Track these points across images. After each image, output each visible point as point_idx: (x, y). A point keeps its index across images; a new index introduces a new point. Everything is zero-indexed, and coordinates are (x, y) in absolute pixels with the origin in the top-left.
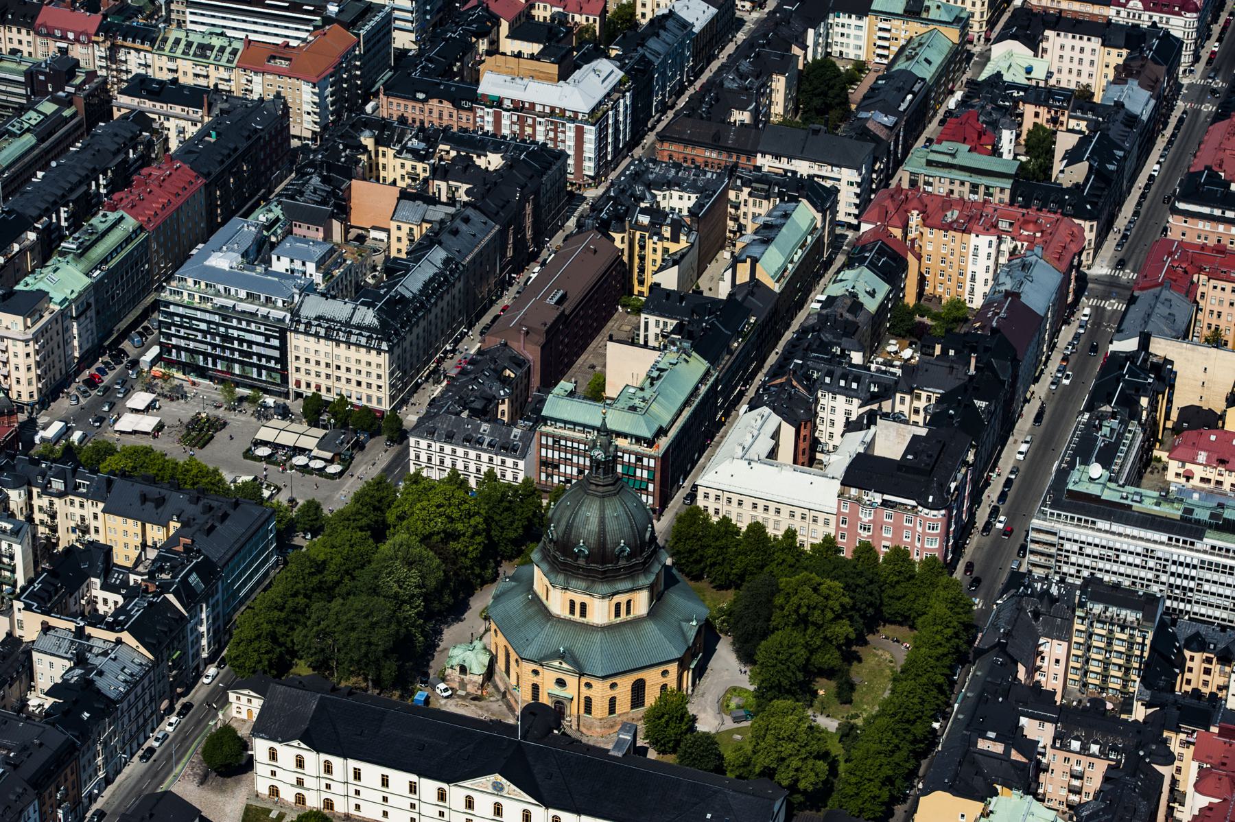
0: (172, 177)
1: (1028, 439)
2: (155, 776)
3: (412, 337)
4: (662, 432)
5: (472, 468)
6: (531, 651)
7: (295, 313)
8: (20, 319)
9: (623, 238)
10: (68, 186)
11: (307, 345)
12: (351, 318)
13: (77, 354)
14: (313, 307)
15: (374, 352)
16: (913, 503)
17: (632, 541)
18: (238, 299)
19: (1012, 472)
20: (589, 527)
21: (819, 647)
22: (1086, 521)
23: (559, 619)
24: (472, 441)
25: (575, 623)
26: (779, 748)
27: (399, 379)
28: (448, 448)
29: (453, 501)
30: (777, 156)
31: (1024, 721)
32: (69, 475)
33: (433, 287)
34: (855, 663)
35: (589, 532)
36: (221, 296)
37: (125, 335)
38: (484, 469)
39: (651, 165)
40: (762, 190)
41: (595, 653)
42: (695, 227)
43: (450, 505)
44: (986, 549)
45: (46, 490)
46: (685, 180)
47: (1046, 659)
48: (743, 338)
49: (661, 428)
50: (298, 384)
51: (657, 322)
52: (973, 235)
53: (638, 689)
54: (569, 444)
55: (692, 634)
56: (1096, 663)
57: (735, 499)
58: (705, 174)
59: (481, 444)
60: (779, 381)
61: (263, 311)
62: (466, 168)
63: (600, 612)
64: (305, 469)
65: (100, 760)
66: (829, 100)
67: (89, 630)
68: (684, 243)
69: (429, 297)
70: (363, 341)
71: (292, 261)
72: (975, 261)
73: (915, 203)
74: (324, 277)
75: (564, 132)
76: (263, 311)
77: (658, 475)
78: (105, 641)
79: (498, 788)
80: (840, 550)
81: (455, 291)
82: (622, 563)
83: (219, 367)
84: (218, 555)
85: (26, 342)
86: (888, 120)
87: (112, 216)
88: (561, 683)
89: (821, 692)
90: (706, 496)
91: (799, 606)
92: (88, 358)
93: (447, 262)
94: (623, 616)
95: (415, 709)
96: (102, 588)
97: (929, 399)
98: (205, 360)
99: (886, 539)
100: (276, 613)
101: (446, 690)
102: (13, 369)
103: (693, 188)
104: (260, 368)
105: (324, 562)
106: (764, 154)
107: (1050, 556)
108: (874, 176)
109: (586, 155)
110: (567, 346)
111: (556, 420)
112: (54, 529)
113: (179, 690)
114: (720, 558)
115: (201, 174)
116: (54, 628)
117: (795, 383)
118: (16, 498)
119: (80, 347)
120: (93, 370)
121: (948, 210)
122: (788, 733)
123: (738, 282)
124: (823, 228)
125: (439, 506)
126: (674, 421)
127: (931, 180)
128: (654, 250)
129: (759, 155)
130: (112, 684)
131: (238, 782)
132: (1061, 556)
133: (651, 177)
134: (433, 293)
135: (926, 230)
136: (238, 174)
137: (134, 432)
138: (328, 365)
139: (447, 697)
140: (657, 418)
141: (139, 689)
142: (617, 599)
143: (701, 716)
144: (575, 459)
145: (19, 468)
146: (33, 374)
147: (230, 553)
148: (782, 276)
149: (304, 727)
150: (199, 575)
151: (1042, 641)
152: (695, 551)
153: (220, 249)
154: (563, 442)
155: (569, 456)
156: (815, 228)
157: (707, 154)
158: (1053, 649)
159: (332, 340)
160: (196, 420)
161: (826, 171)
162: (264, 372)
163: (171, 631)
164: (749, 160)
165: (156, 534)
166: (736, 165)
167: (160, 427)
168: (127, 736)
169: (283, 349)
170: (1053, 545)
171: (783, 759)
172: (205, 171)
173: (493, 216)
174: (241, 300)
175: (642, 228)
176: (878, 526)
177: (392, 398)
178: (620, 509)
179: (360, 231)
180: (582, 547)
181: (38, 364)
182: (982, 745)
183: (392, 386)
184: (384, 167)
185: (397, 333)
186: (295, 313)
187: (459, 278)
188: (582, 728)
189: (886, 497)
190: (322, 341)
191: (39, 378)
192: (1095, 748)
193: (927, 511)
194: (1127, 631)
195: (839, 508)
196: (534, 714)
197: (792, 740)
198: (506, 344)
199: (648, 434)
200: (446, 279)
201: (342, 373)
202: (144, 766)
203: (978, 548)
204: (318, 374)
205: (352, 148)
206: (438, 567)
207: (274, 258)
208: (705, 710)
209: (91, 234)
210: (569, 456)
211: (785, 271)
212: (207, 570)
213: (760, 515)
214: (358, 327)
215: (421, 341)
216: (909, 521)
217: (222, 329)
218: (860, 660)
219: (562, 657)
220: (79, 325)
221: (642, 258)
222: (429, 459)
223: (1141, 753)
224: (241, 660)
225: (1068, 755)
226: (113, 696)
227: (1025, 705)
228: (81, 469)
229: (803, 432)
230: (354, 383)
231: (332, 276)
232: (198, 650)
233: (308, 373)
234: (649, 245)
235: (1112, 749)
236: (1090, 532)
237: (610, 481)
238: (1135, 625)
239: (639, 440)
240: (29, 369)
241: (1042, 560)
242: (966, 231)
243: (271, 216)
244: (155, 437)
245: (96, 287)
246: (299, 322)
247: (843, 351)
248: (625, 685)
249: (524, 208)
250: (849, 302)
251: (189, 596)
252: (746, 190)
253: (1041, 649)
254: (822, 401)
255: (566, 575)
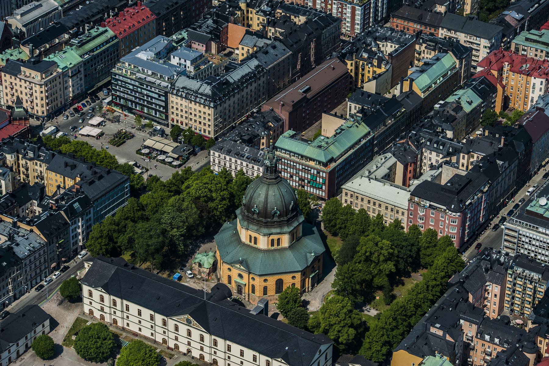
0: (139, 14)
1: (535, 185)
2: (40, 299)
3: (231, 102)
4: (332, 160)
5: (233, 167)
6: (228, 258)
7: (173, 84)
8: (39, 74)
9: (352, 64)
10: (91, 14)
11: (177, 101)
12: (199, 90)
13: (71, 95)
14: (182, 82)
15: (207, 107)
16: (445, 208)
17: (281, 208)
18: (147, 75)
19: (520, 201)
20: (260, 199)
21: (377, 274)
22: (534, 227)
23: (244, 244)
24: (239, 155)
25: (252, 247)
26: (330, 320)
27: (221, 123)
28: (228, 158)
29: (213, 182)
30: (449, 30)
31: (462, 321)
32: (36, 150)
33: (246, 79)
34: (400, 286)
35: (260, 202)
36: (140, 73)
37: (100, 89)
38: (239, 168)
39: (379, 28)
40: (433, 46)
41: (257, 262)
42: (390, 61)
43: (211, 184)
44: (491, 237)
45: (24, 157)
46: (394, 37)
47: (490, 294)
48: (395, 119)
49: (333, 158)
50: (173, 120)
51: (355, 107)
52: (533, 78)
53: (279, 283)
54: (286, 161)
55: (310, 260)
56: (517, 299)
57: (360, 197)
58: (405, 35)
59: (243, 157)
60: (402, 141)
61: (158, 82)
62: (285, 22)
63: (263, 243)
64: (163, 161)
65: (10, 287)
66: (497, 4)
67: (19, 224)
68: (383, 69)
69: (242, 83)
70: (202, 101)
71: (180, 59)
72: (533, 92)
73: (507, 58)
74: (195, 68)
75: (346, 9)
76: (158, 82)
77: (327, 182)
78: (26, 230)
79: (189, 322)
80: (403, 228)
81: (261, 82)
82: (276, 219)
83: (138, 109)
84: (93, 196)
85: (41, 85)
86: (518, 16)
87: (101, 29)
88: (240, 276)
89: (378, 298)
90: (346, 194)
91: (366, 252)
92: (78, 98)
93: (257, 67)
94: (276, 246)
95: (172, 283)
96: (38, 206)
97: (478, 157)
98: (132, 104)
99: (431, 225)
100: (114, 227)
101: (190, 274)
102: (34, 98)
103: (398, 42)
104: (156, 110)
105: (146, 205)
106: (443, 28)
107: (515, 243)
108: (502, 45)
109: (357, 22)
110: (308, 114)
111: (282, 149)
112: (28, 176)
113: (63, 259)
114: (343, 225)
115: (153, 13)
116: (4, 221)
117: (410, 143)
118: (10, 159)
119: (73, 92)
120: (80, 104)
121: (524, 64)
122: (335, 312)
123: (403, 91)
124: (461, 68)
125: (205, 184)
126: (341, 155)
127: (526, 48)
128: (369, 71)
129: (440, 29)
130: (22, 251)
131: (77, 306)
132: (519, 244)
133: (377, 34)
134: (246, 81)
135: (511, 73)
136: (177, 16)
137: (88, 136)
138: (186, 112)
139: (191, 278)
140: (332, 152)
141: (37, 255)
142: (272, 237)
143: (313, 302)
144: (289, 170)
145: (15, 144)
146: (44, 102)
147: (100, 195)
148: (428, 90)
149: (106, 281)
150: (79, 204)
151: (488, 284)
152: (332, 220)
153: (146, 50)
154: (283, 160)
155: (286, 168)
156: (455, 67)
157: (415, 26)
158: (494, 289)
159: (188, 99)
160: (119, 132)
161: (473, 39)
162: (158, 113)
163: (59, 229)
164: (435, 31)
165: (70, 183)
166: (421, 32)
167: (101, 135)
168: (29, 277)
169: (166, 102)
170: (515, 238)
171: (332, 325)
172: (157, 12)
173: (290, 47)
174: (149, 76)
175: (364, 59)
176: (426, 217)
177: (215, 132)
178: (277, 192)
179: (231, 50)
180: (255, 209)
181: (47, 97)
182: (433, 330)
183: (216, 126)
184: (251, 19)
185: (220, 99)
186: (173, 84)
187: (263, 76)
188: (251, 301)
189: (432, 203)
190: (184, 99)
191: (48, 104)
192: (497, 340)
193: (450, 213)
194: (533, 284)
195: (409, 207)
196: (218, 289)
197: (338, 316)
198: (272, 110)
199: (324, 160)
200: (255, 75)
201: (192, 117)
202: (37, 293)
203: (487, 237)
204: (204, 118)
205: (233, 7)
206: (195, 213)
207: (172, 57)
208: (315, 299)
209: (88, 37)
210: (286, 168)
211: (430, 87)
212: (85, 202)
213: (365, 206)
214: (201, 94)
215: (236, 106)
216: (442, 217)
217: (139, 89)
218: (403, 284)
219: (241, 263)
220: (73, 81)
221: (363, 75)
222: (219, 162)
223: (517, 345)
224: (92, 248)
225: (484, 342)
226: (21, 256)
227: (464, 313)
228: (43, 148)
229: (410, 168)
230: (198, 122)
231: (200, 69)
232: (76, 241)
233: (177, 115)
234: (367, 69)
235: (505, 342)
236: (534, 233)
237: (273, 177)
238: (537, 281)
239: (320, 163)
240: (42, 99)
241: (511, 245)
242: (529, 75)
243: (180, 37)
244: (97, 139)
245: (85, 63)
246: (174, 89)
247: (443, 130)
248: (272, 281)
249: (310, 45)
250: (454, 106)
251: (71, 212)
252: (424, 45)
253: (488, 288)
254: (425, 154)
255: (248, 222)
